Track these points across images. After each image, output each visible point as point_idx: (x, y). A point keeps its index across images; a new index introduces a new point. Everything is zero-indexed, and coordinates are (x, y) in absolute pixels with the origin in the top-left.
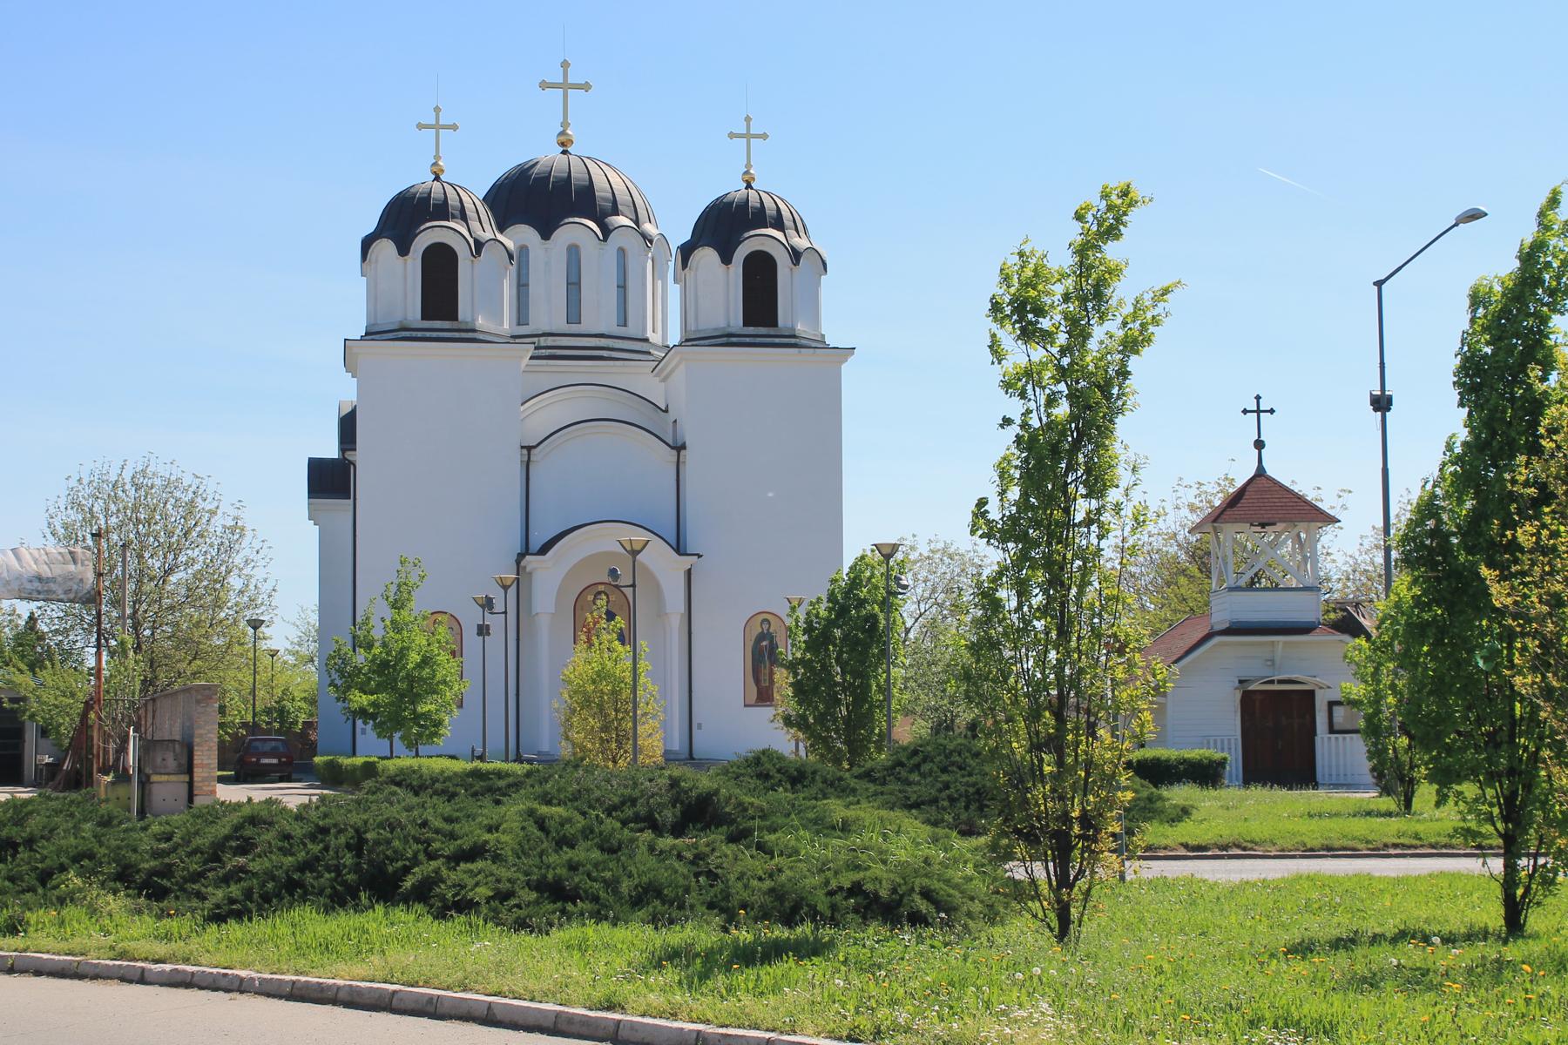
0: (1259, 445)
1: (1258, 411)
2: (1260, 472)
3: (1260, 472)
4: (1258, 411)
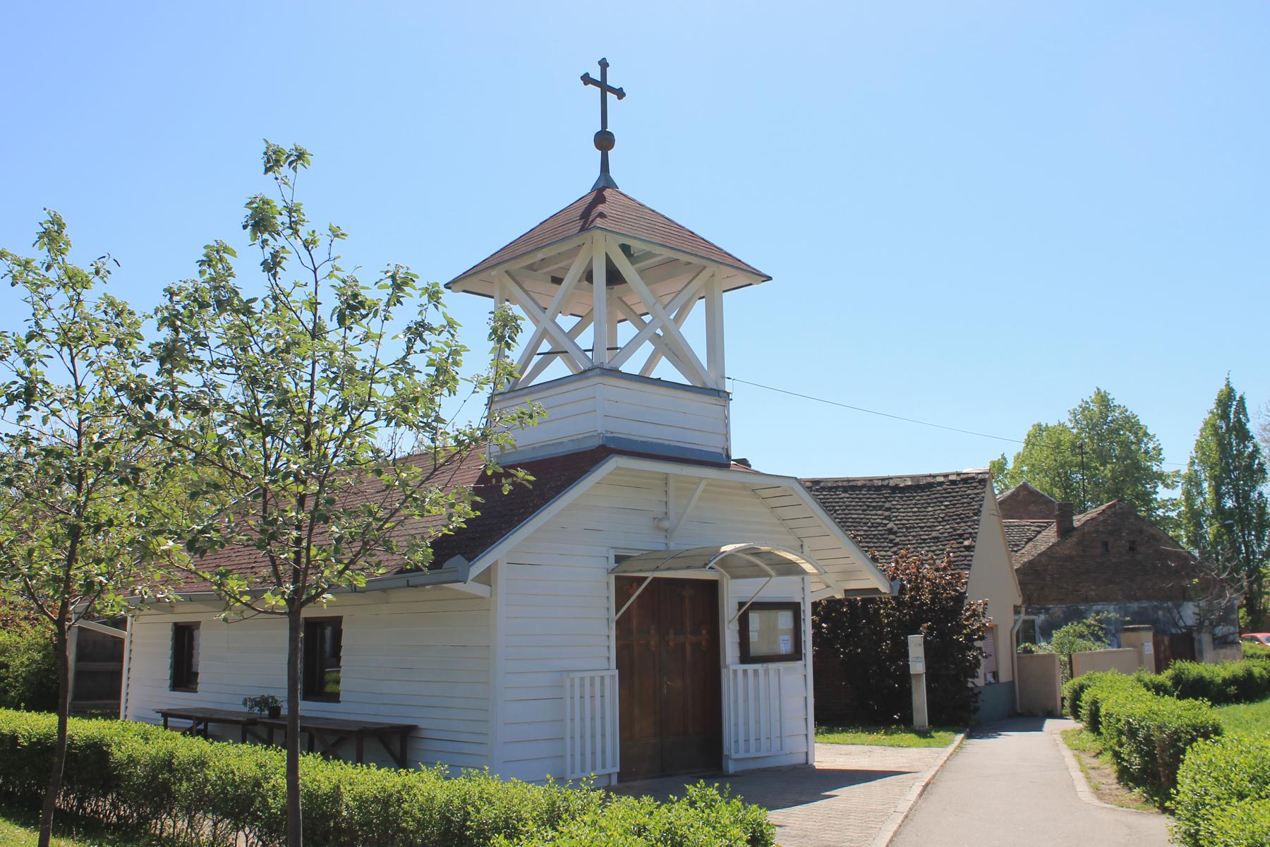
0: (604, 141)
1: (603, 86)
2: (605, 183)
3: (605, 183)
4: (603, 86)
